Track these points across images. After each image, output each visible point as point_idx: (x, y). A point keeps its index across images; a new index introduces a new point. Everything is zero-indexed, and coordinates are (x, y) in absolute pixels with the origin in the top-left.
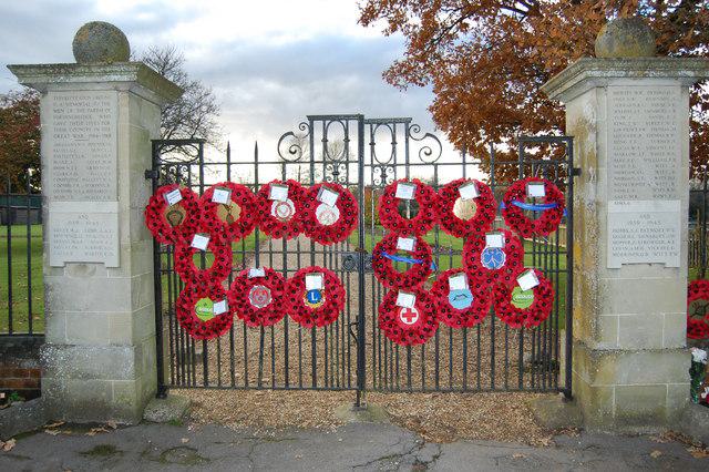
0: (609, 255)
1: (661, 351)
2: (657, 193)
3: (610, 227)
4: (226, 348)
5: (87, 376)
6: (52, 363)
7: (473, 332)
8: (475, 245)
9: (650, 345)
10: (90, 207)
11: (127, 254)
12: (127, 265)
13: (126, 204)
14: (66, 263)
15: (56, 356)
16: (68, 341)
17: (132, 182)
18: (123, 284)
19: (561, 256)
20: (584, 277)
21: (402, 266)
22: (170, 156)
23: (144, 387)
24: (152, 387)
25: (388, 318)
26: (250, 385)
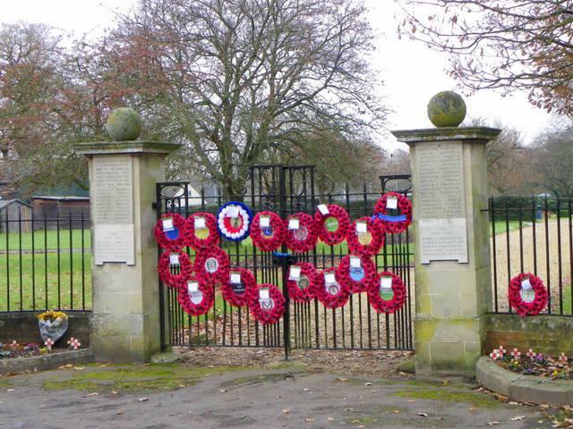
0: (421, 255)
1: (459, 320)
2: (450, 213)
3: (421, 237)
4: (347, 315)
5: (116, 334)
6: (96, 325)
7: (338, 310)
8: (353, 238)
9: (453, 316)
10: (118, 227)
11: (139, 258)
12: (139, 264)
13: (139, 225)
14: (104, 263)
15: (98, 321)
16: (105, 312)
17: (142, 211)
18: (136, 276)
19: (391, 252)
20: (131, 371)
21: (302, 236)
22: (167, 191)
23: (150, 343)
24: (157, 344)
25: (334, 207)
26: (567, 204)
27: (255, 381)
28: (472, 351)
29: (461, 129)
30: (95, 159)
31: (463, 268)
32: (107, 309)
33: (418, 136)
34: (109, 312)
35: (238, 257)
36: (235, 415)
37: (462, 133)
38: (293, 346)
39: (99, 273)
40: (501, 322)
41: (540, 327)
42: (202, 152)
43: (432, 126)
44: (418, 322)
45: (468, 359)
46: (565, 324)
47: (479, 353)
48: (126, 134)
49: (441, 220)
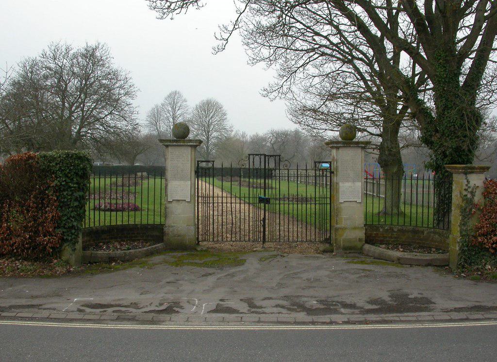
5: (179, 236)
27: (119, 306)
28: (360, 240)
29: (354, 142)
30: (170, 148)
31: (359, 205)
32: (174, 223)
33: (343, 144)
34: (175, 225)
35: (213, 203)
36: (481, 170)
37: (363, 144)
38: (267, 240)
39: (169, 205)
40: (371, 228)
41: (389, 231)
42: (89, 141)
43: (340, 139)
44: (337, 230)
45: (359, 245)
46: (403, 229)
47: (364, 242)
48: (241, 139)
49: (350, 183)
